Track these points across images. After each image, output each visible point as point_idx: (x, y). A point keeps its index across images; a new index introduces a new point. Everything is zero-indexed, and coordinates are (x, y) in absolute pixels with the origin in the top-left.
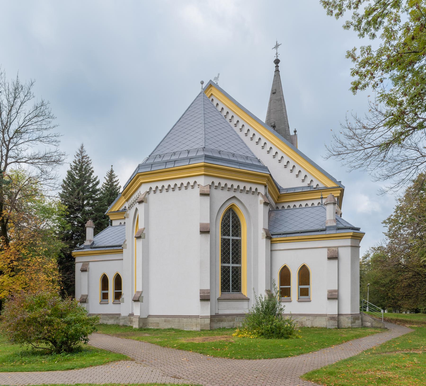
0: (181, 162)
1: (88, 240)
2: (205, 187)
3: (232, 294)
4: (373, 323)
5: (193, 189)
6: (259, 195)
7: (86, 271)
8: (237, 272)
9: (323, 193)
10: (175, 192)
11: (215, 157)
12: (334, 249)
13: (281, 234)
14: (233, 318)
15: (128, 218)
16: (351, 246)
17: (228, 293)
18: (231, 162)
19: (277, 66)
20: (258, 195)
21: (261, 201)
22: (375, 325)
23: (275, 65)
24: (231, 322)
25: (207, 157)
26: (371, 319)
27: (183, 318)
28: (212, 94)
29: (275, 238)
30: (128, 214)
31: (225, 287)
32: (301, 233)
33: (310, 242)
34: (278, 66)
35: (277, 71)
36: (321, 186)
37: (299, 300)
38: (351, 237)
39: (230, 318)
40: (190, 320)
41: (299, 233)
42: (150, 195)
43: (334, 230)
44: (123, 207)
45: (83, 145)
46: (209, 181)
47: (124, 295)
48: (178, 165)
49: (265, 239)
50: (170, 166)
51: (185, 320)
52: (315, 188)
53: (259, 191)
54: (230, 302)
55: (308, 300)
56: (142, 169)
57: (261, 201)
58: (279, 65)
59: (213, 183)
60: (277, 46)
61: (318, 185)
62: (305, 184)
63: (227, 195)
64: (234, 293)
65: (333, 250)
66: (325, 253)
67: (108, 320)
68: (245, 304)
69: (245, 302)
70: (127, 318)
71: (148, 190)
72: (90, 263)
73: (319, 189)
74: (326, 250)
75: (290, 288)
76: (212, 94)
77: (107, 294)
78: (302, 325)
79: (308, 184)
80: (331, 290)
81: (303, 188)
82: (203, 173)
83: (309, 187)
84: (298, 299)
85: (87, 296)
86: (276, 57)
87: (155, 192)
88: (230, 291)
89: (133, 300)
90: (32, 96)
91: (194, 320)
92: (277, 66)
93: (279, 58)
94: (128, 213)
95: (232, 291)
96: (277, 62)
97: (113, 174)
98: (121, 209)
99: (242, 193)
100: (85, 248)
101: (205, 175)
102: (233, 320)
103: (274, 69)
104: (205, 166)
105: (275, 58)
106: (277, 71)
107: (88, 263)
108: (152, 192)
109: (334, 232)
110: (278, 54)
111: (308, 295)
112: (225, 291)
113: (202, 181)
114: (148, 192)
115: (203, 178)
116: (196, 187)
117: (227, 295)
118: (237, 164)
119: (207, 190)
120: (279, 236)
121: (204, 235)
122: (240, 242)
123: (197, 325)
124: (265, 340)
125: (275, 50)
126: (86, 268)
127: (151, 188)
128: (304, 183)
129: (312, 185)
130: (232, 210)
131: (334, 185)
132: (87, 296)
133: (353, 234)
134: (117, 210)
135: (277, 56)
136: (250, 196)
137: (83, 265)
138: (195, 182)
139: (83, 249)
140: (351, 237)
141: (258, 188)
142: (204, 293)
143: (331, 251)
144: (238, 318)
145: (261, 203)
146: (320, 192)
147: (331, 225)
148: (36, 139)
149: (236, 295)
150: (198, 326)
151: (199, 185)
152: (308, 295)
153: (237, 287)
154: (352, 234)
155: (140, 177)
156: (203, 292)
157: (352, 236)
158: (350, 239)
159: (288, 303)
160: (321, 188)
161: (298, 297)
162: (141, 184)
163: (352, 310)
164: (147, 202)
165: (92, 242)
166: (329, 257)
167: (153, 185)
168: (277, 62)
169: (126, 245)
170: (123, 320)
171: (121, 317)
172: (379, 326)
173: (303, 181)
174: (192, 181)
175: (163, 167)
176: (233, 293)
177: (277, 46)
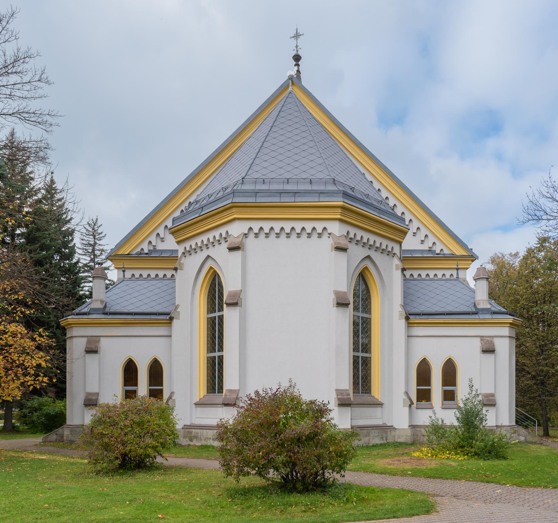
0: (333, 196)
1: (97, 300)
2: (340, 239)
4: (527, 437)
5: (320, 239)
6: (394, 257)
7: (96, 352)
9: (459, 262)
10: (268, 239)
11: (357, 197)
12: (489, 339)
13: (419, 314)
14: (369, 431)
15: (181, 269)
16: (509, 337)
17: (357, 395)
18: (369, 206)
19: (297, 65)
20: (393, 256)
21: (396, 265)
22: (529, 440)
23: (295, 63)
24: (366, 437)
25: (345, 195)
26: (525, 432)
29: (413, 319)
30: (183, 264)
32: (447, 314)
33: (494, 327)
36: (446, 251)
37: (444, 406)
38: (509, 325)
39: (365, 432)
41: (444, 314)
42: (247, 239)
43: (488, 315)
44: (139, 249)
45: (15, 131)
46: (345, 229)
47: (175, 395)
48: (300, 201)
49: (404, 320)
50: (287, 200)
52: (438, 254)
53: (395, 251)
54: (363, 408)
56: (239, 197)
57: (396, 265)
58: (299, 63)
59: (348, 233)
60: (297, 36)
61: (442, 250)
62: (425, 247)
63: (365, 252)
64: (364, 395)
65: (488, 341)
66: (477, 344)
69: (378, 408)
71: (246, 232)
72: (102, 339)
73: (446, 256)
74: (477, 341)
75: (429, 390)
79: (430, 248)
80: (486, 394)
81: (422, 251)
82: (339, 217)
83: (430, 252)
84: (442, 404)
85: (98, 394)
86: (295, 51)
87: (257, 235)
89: (381, 405)
90: (14, 38)
93: (300, 53)
94: (182, 261)
95: (218, 393)
96: (297, 58)
97: (54, 186)
98: (134, 253)
99: (377, 252)
100: (91, 312)
101: (340, 220)
102: (368, 435)
104: (343, 208)
105: (294, 53)
107: (99, 337)
108: (252, 236)
109: (488, 316)
110: (298, 48)
113: (336, 228)
114: (245, 234)
115: (336, 225)
116: (325, 235)
117: (208, 395)
118: (376, 209)
119: (343, 242)
120: (418, 317)
121: (341, 309)
122: (370, 322)
124: (481, 463)
125: (293, 41)
126: (97, 347)
127: (251, 229)
128: (423, 245)
129: (434, 249)
130: (362, 275)
131: (464, 253)
132: (98, 394)
133: (513, 321)
134: (127, 253)
135: (297, 51)
136: (385, 257)
137: (88, 342)
138: (325, 229)
139: (89, 314)
140: (509, 325)
141: (394, 247)
142: (342, 394)
143: (486, 342)
144: (373, 431)
145: (397, 269)
146: (456, 260)
147: (485, 307)
148: (13, 114)
151: (330, 234)
154: (511, 322)
155: (234, 209)
156: (341, 393)
157: (510, 324)
158: (508, 328)
159: (428, 410)
160: (446, 254)
161: (442, 402)
162: (235, 219)
163: (510, 422)
164: (243, 250)
165: (104, 304)
166: (484, 349)
167: (256, 226)
169: (179, 314)
172: (534, 441)
173: (422, 242)
174: (320, 227)
175: (277, 199)
176: (362, 395)
177: (297, 36)
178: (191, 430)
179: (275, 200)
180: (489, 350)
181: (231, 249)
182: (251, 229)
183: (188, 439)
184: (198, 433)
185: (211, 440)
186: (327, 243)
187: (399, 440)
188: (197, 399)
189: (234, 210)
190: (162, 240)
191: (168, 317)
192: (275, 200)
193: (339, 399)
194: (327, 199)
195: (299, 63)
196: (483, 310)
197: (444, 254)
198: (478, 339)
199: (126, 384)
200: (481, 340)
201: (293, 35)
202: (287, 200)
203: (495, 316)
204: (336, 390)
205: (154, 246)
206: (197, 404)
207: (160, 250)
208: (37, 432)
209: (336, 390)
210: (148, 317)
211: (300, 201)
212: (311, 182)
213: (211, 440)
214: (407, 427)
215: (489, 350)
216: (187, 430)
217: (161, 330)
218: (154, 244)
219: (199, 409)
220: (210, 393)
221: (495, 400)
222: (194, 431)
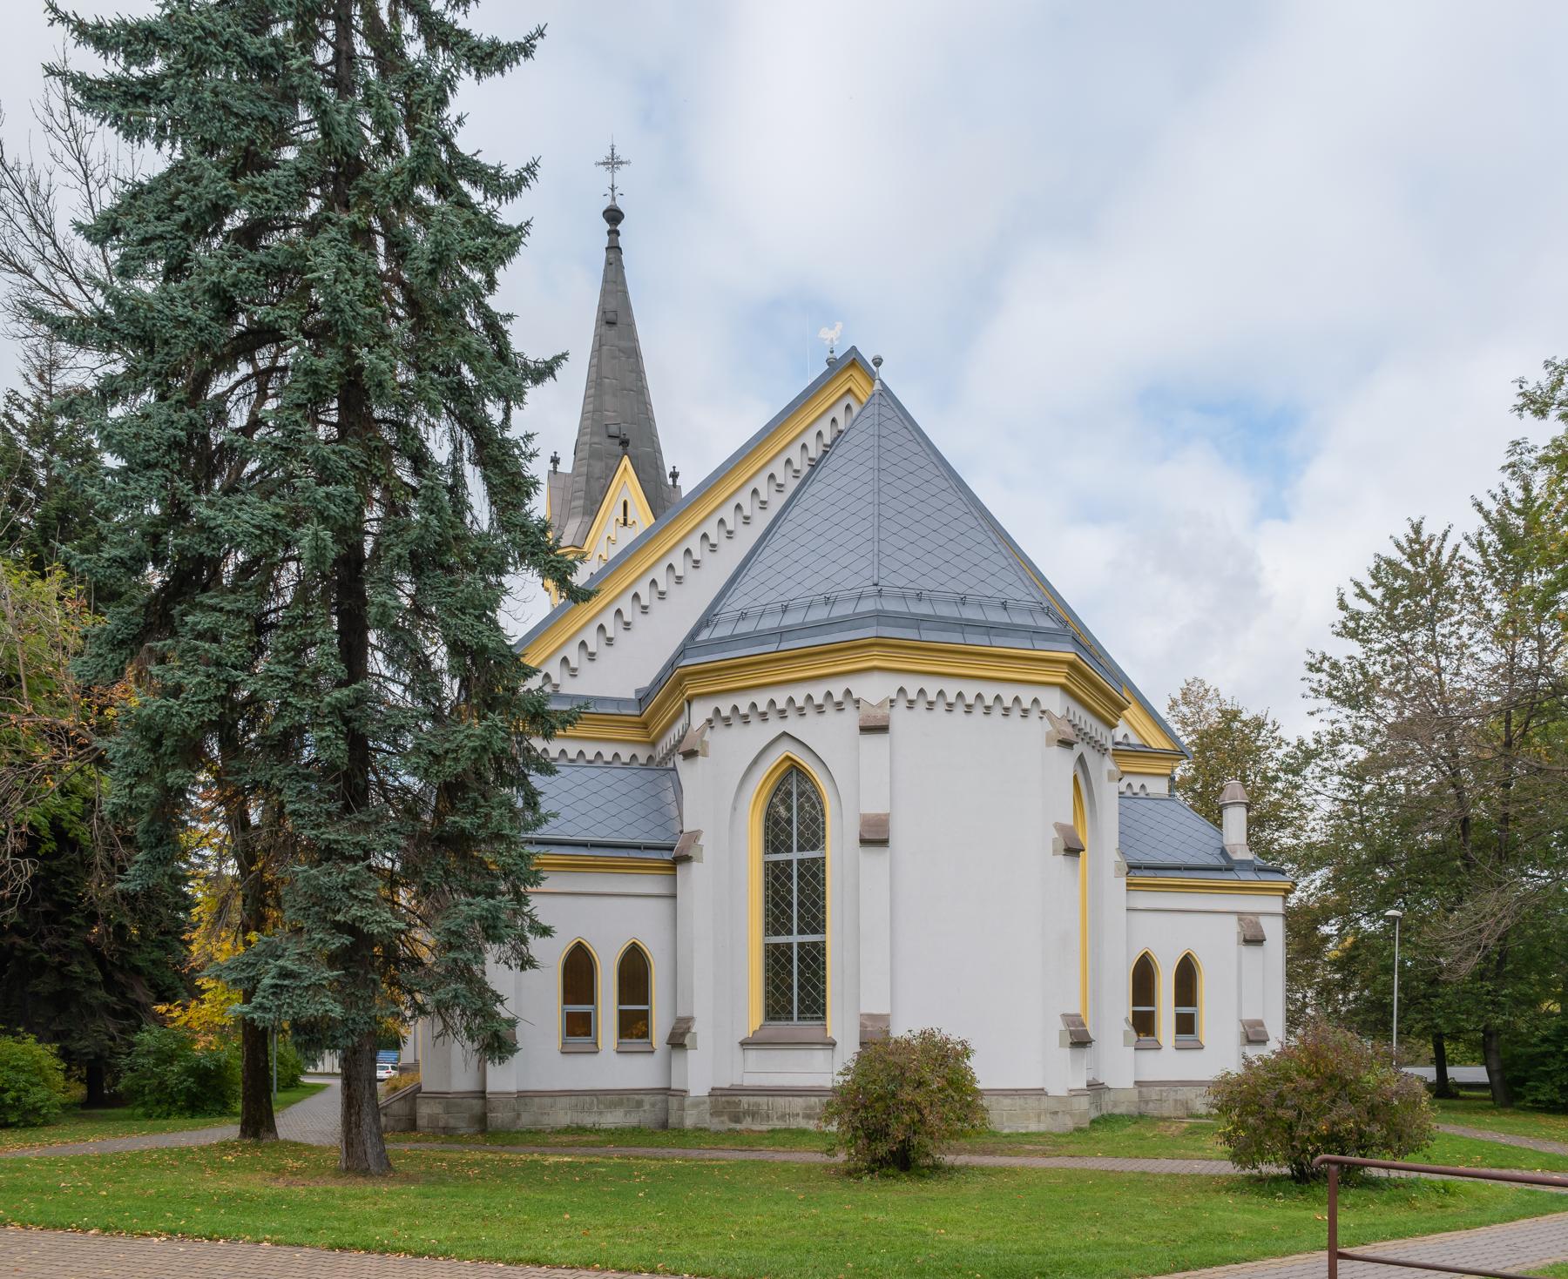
0: (1055, 641)
3: (796, 1027)
8: (814, 958)
10: (971, 717)
15: (705, 755)
19: (614, 233)
21: (1110, 772)
23: (608, 227)
27: (1001, 1098)
28: (849, 390)
31: (776, 1007)
34: (618, 233)
35: (614, 248)
36: (1134, 740)
37: (1181, 1044)
40: (1019, 1102)
41: (1178, 869)
48: (1002, 645)
51: (1007, 1101)
55: (1194, 1044)
57: (1110, 772)
58: (619, 228)
61: (1126, 736)
66: (1231, 927)
67: (601, 1113)
68: (819, 1057)
70: (705, 1102)
76: (849, 390)
77: (644, 1016)
78: (1187, 1109)
82: (1063, 680)
88: (792, 1019)
91: (1032, 1102)
92: (614, 233)
93: (621, 204)
95: (799, 1019)
96: (614, 216)
101: (1063, 687)
103: (605, 241)
106: (614, 248)
109: (1251, 876)
110: (616, 192)
111: (588, 1034)
112: (780, 1019)
113: (1054, 702)
114: (892, 701)
116: (1035, 714)
117: (781, 1028)
123: (1039, 1116)
125: (604, 174)
135: (614, 199)
142: (1073, 1023)
149: (807, 1029)
150: (1042, 1117)
151: (1043, 712)
152: (588, 1034)
153: (814, 1006)
167: (912, 686)
168: (614, 216)
170: (694, 1112)
171: (688, 1102)
174: (1027, 695)
177: (613, 163)
178: (736, 1099)
179: (954, 638)
180: (1254, 940)
181: (865, 730)
182: (901, 690)
183: (725, 1118)
184: (758, 1105)
185: (800, 1119)
186: (1037, 729)
187: (1117, 1111)
188: (747, 1033)
189: (875, 651)
190: (573, 673)
191: (667, 856)
192: (954, 638)
193: (1071, 1033)
194: (1046, 645)
195: (619, 228)
196: (1241, 862)
197: (1129, 745)
198: (1234, 918)
199: (567, 1000)
200: (1240, 920)
201: (603, 159)
202: (977, 641)
203: (1263, 876)
204: (1064, 1016)
205: (556, 686)
206: (745, 1044)
207: (567, 696)
208: (169, 1114)
209: (1064, 1016)
210: (634, 853)
211: (1002, 645)
212: (1004, 606)
213: (800, 1119)
214: (1131, 1085)
215: (1254, 940)
216: (724, 1099)
217: (652, 884)
218: (555, 681)
219: (753, 1055)
220: (773, 1019)
221: (1265, 1034)
222: (745, 1100)
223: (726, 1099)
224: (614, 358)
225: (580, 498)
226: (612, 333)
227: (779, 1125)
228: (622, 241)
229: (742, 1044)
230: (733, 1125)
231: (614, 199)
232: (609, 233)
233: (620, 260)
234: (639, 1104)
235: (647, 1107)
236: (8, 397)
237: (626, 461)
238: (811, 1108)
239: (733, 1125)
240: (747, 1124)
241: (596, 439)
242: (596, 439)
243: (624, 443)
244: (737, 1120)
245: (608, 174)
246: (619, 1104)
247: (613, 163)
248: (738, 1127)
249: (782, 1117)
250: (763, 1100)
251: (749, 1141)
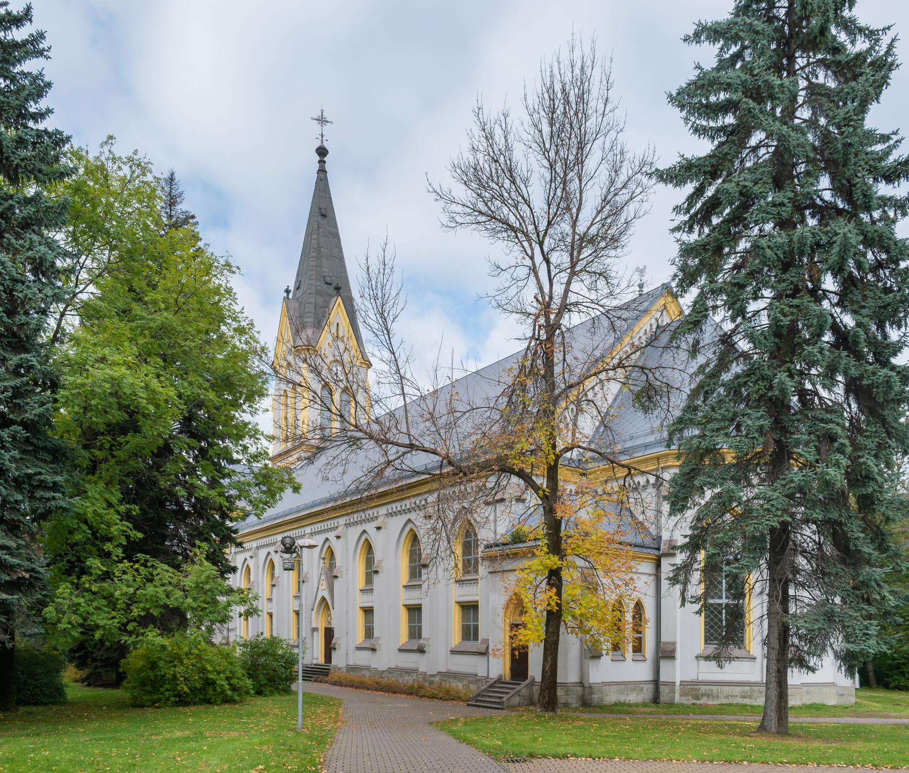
19: (322, 162)
23: (318, 158)
34: (324, 162)
35: (322, 171)
68: (745, 665)
92: (322, 162)
93: (326, 145)
96: (322, 152)
103: (317, 166)
106: (322, 171)
135: (322, 142)
168: (322, 152)
178: (697, 687)
183: (690, 698)
206: (400, 650)
222: (703, 688)
223: (691, 687)
224: (327, 236)
225: (310, 317)
226: (323, 221)
227: (724, 701)
228: (328, 167)
229: (697, 657)
230: (695, 701)
231: (322, 142)
232: (319, 162)
233: (326, 179)
234: (642, 689)
235: (645, 691)
236: (193, 217)
237: (340, 300)
238: (745, 692)
239: (695, 701)
240: (704, 701)
241: (319, 283)
242: (319, 283)
243: (337, 289)
244: (697, 698)
245: (319, 126)
246: (634, 690)
247: (322, 120)
248: (698, 702)
249: (727, 697)
250: (715, 688)
251: (704, 710)
